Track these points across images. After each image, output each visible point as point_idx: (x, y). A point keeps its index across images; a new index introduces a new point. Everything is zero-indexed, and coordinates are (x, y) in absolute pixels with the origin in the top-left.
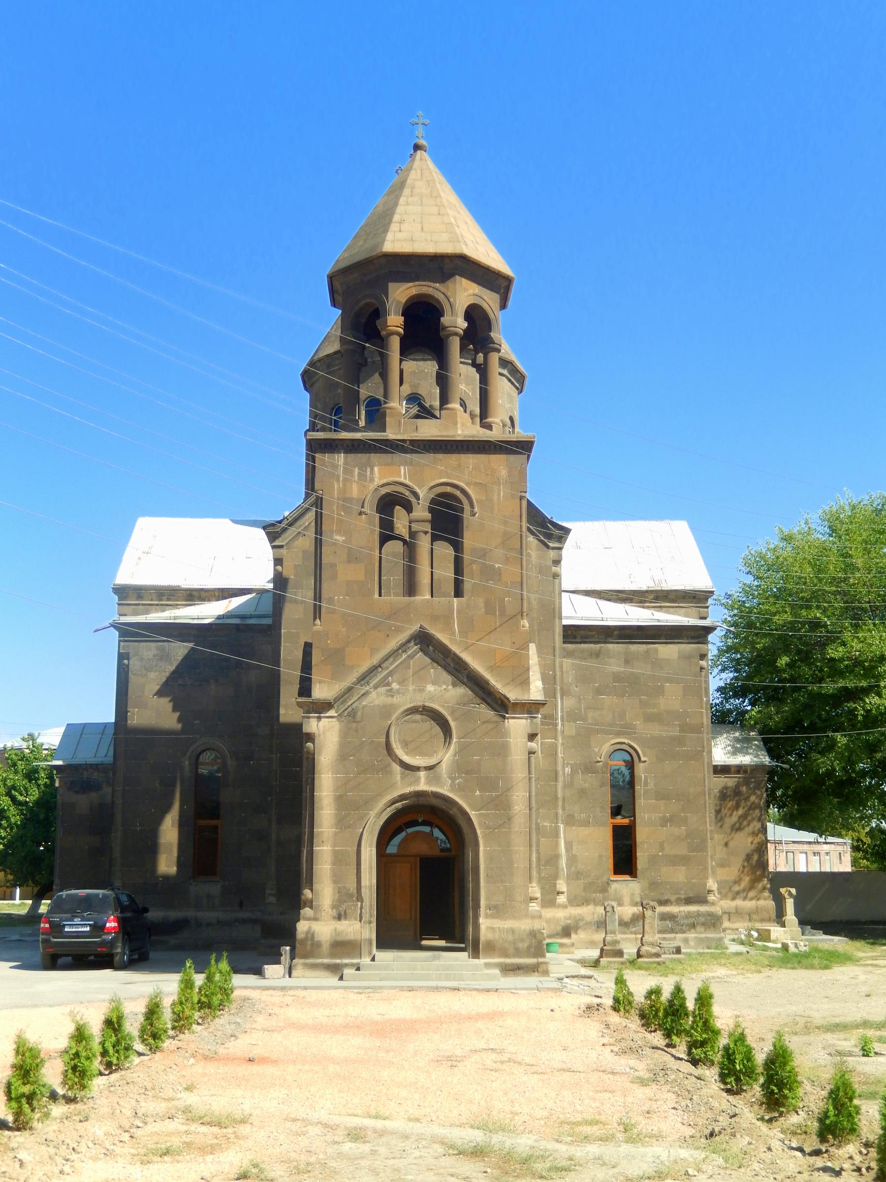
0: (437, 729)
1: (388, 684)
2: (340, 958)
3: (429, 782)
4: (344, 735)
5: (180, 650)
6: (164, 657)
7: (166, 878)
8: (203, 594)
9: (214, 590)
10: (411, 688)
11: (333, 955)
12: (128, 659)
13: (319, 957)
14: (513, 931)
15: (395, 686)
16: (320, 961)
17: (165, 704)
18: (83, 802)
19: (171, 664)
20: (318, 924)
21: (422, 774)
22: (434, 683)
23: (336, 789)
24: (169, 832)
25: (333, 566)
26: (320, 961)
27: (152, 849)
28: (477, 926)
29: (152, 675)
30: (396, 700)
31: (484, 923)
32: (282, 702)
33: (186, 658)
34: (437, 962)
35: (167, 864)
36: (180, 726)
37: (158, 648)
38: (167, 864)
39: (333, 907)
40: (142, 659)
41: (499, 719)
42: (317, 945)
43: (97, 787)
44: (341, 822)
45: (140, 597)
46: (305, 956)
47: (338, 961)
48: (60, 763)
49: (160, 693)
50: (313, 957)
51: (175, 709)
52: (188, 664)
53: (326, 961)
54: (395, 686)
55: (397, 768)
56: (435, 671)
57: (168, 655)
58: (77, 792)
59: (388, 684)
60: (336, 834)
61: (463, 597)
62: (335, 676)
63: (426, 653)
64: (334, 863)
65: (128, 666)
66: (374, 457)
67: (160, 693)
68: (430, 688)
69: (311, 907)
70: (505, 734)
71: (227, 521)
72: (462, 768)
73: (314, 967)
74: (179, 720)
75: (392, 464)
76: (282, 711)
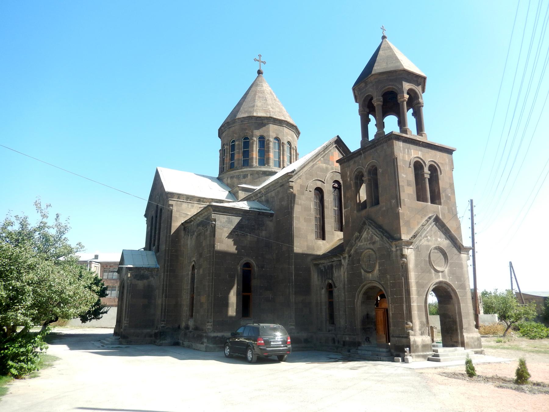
0: (442, 256)
1: (427, 237)
2: (425, 352)
3: (443, 278)
4: (416, 256)
5: (236, 220)
6: (230, 222)
7: (231, 317)
8: (205, 200)
9: (209, 199)
10: (434, 239)
11: (423, 351)
12: (215, 221)
13: (418, 352)
14: (473, 338)
15: (429, 238)
16: (419, 354)
17: (231, 242)
18: (141, 284)
19: (233, 225)
20: (418, 338)
21: (440, 274)
22: (440, 238)
23: (416, 279)
24: (233, 297)
25: (403, 186)
26: (419, 354)
27: (226, 304)
28: (462, 337)
29: (225, 229)
30: (430, 243)
31: (465, 335)
32: (295, 245)
33: (239, 224)
34: (456, 352)
35: (232, 311)
36: (236, 252)
37: (227, 218)
38: (232, 311)
39: (420, 330)
40: (221, 222)
41: (458, 253)
42: (417, 346)
43: (147, 278)
44: (419, 293)
45: (179, 198)
46: (414, 352)
47: (425, 353)
48: (132, 266)
49: (228, 237)
50: (417, 352)
51: (234, 244)
52: (239, 226)
53: (422, 353)
54: (429, 238)
55: (433, 271)
56: (440, 233)
57: (231, 221)
58: (138, 280)
59: (427, 237)
60: (417, 298)
61: (440, 204)
62: (408, 233)
63: (436, 226)
64: (418, 311)
65: (215, 225)
66: (412, 146)
67: (228, 237)
68: (439, 240)
69: (412, 330)
70: (461, 259)
71: (193, 174)
72: (452, 273)
73: (418, 356)
74: (236, 249)
75: (416, 150)
76: (295, 248)
